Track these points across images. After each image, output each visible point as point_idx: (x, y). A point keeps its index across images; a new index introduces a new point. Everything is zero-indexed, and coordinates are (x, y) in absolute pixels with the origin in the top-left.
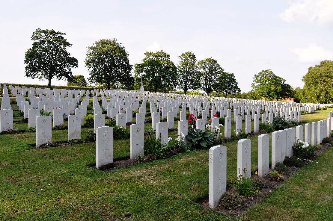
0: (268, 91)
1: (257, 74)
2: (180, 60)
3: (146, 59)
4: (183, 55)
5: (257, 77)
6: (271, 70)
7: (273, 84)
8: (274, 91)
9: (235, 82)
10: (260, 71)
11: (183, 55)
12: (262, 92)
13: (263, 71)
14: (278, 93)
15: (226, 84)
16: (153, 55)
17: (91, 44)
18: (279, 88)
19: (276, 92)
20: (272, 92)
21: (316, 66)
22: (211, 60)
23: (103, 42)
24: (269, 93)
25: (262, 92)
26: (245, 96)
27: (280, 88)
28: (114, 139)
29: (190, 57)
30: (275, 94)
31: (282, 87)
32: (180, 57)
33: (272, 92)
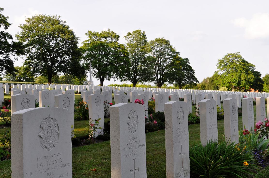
0: (239, 81)
1: (221, 58)
2: (86, 38)
3: (88, 41)
4: (129, 34)
5: (221, 62)
6: (239, 53)
7: (244, 71)
8: (246, 81)
9: (190, 69)
10: (226, 54)
11: (129, 34)
12: (229, 83)
13: (229, 55)
14: (250, 83)
15: (180, 72)
16: (96, 35)
17: (24, 23)
18: (251, 76)
19: (247, 81)
20: (244, 82)
21: (10, 35)
22: (163, 40)
23: (40, 20)
24: (239, 83)
25: (229, 83)
26: (203, 87)
27: (253, 76)
28: (218, 119)
29: (141, 37)
30: (247, 84)
31: (255, 76)
32: (126, 37)
33: (244, 82)
